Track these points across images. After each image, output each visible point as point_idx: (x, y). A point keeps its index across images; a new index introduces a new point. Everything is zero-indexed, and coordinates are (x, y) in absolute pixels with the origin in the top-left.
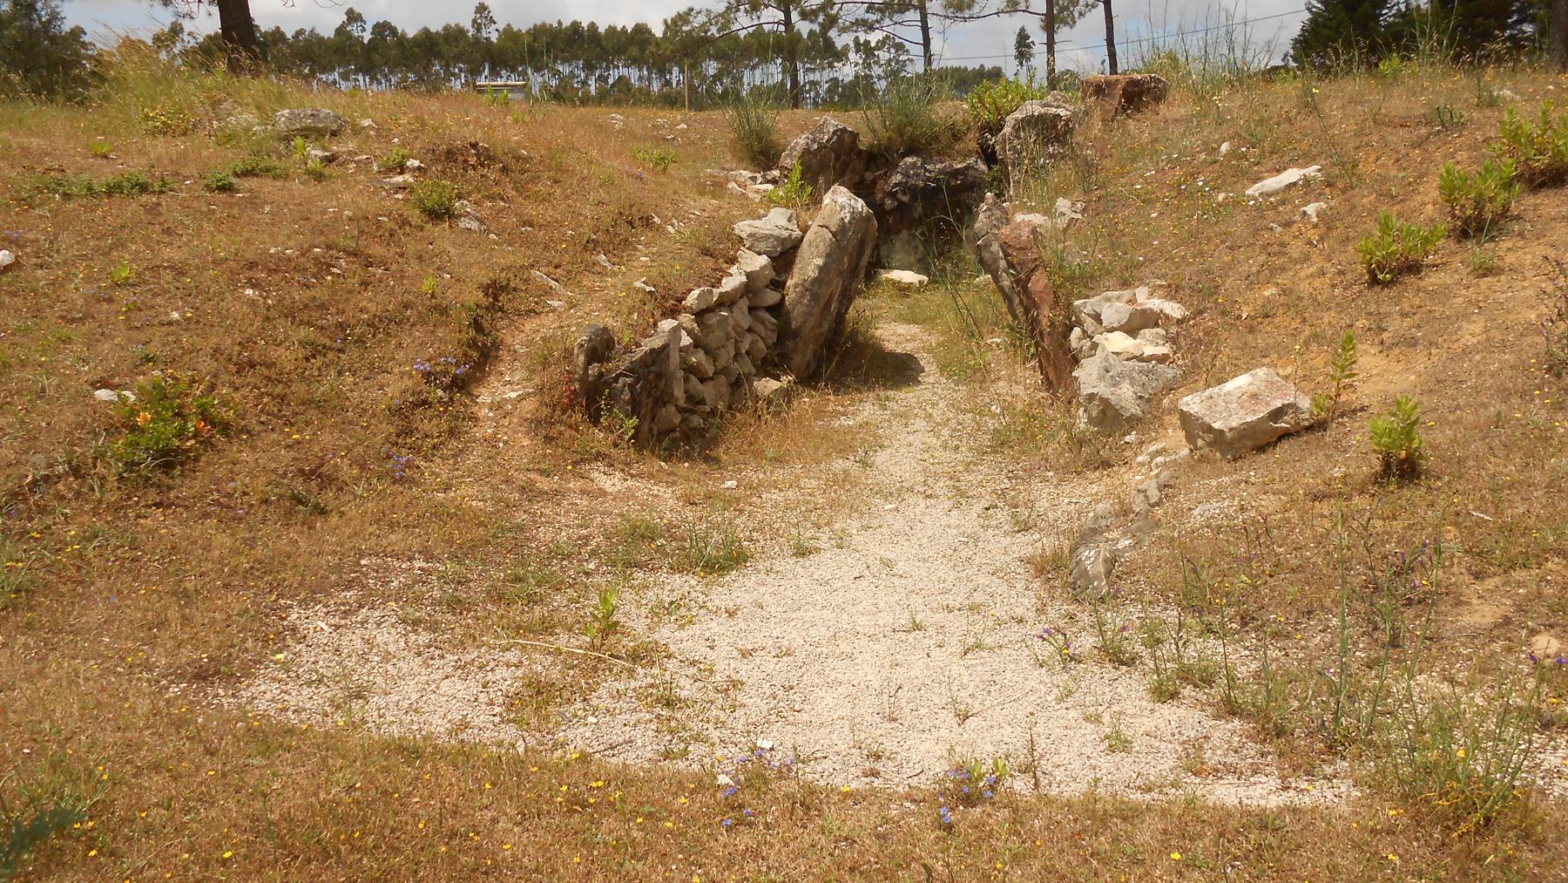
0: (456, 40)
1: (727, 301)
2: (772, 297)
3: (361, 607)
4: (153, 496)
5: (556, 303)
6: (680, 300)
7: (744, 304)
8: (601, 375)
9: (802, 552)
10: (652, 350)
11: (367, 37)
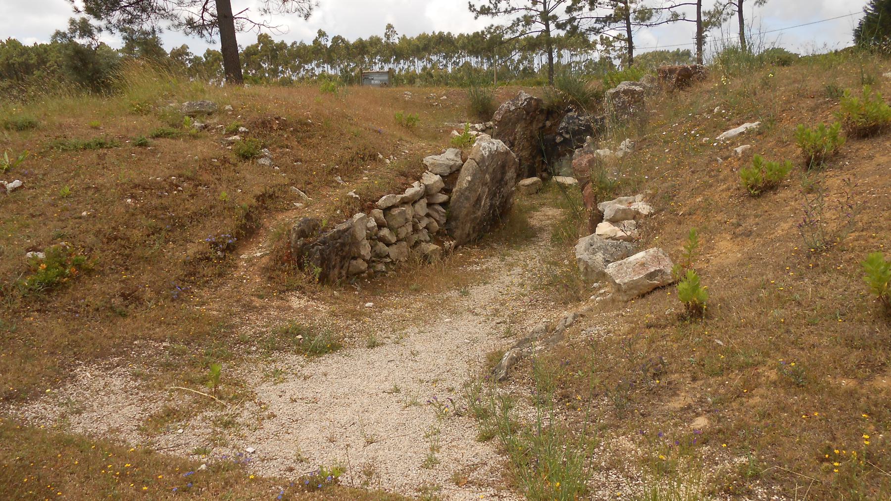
0: (376, 44)
1: (412, 201)
2: (443, 198)
3: (118, 365)
4: (37, 306)
5: (298, 205)
6: (374, 202)
7: (424, 202)
8: (304, 244)
9: (373, 345)
10: (339, 231)
11: (329, 44)
